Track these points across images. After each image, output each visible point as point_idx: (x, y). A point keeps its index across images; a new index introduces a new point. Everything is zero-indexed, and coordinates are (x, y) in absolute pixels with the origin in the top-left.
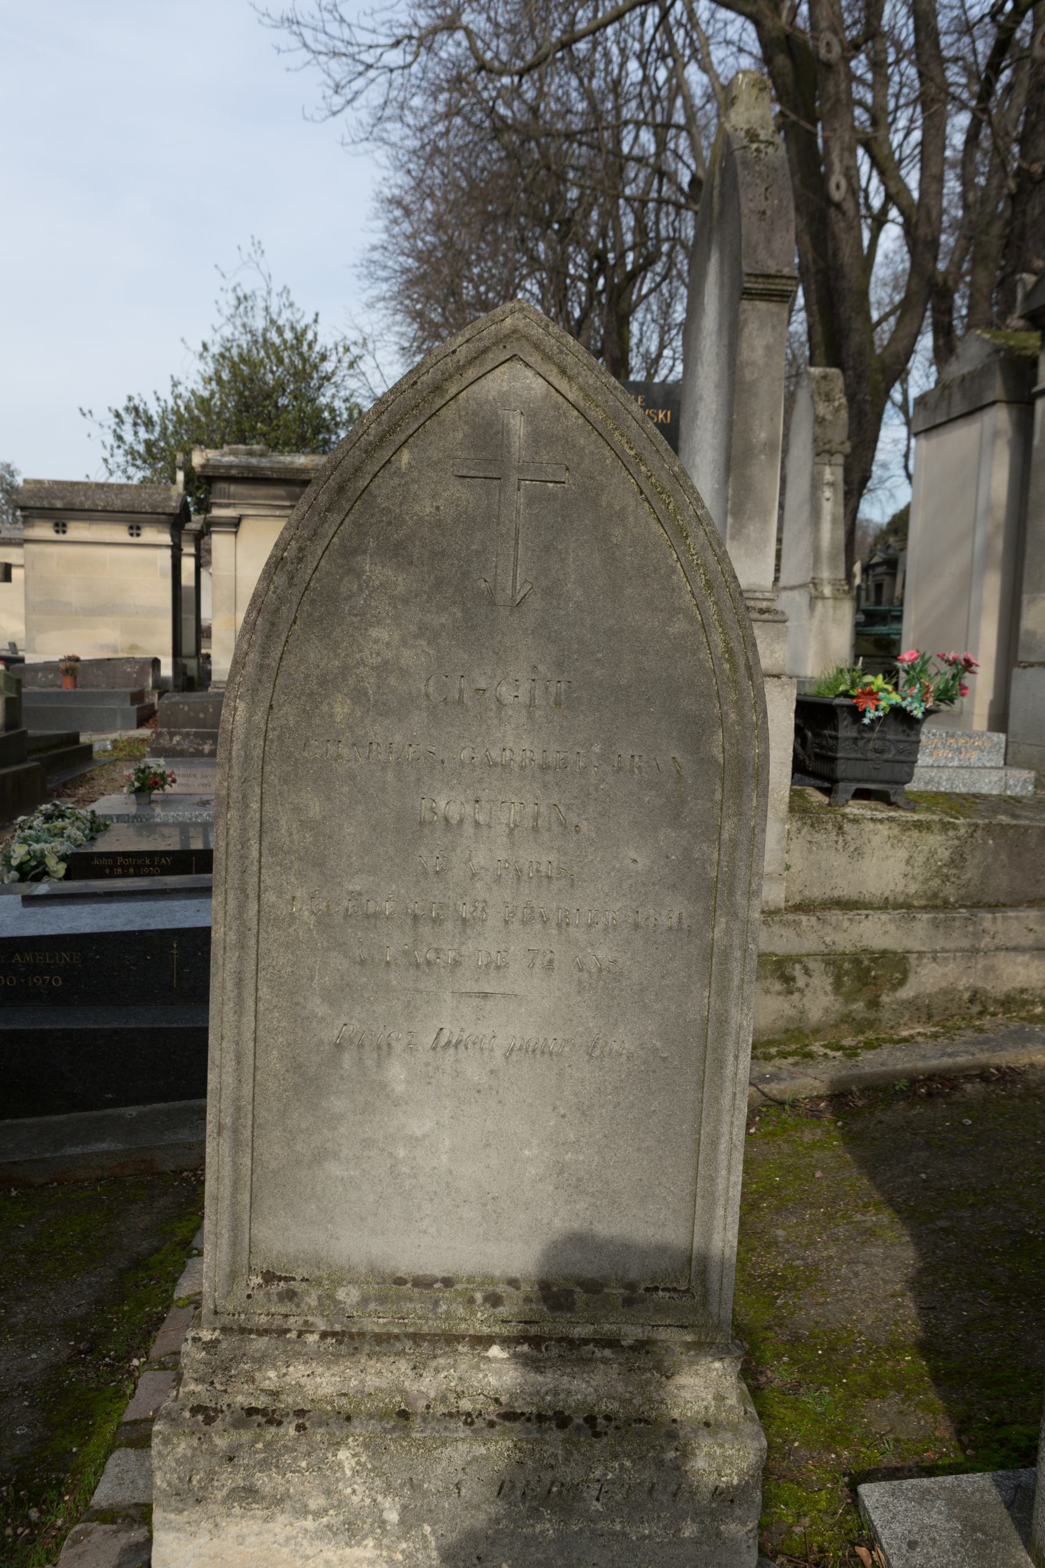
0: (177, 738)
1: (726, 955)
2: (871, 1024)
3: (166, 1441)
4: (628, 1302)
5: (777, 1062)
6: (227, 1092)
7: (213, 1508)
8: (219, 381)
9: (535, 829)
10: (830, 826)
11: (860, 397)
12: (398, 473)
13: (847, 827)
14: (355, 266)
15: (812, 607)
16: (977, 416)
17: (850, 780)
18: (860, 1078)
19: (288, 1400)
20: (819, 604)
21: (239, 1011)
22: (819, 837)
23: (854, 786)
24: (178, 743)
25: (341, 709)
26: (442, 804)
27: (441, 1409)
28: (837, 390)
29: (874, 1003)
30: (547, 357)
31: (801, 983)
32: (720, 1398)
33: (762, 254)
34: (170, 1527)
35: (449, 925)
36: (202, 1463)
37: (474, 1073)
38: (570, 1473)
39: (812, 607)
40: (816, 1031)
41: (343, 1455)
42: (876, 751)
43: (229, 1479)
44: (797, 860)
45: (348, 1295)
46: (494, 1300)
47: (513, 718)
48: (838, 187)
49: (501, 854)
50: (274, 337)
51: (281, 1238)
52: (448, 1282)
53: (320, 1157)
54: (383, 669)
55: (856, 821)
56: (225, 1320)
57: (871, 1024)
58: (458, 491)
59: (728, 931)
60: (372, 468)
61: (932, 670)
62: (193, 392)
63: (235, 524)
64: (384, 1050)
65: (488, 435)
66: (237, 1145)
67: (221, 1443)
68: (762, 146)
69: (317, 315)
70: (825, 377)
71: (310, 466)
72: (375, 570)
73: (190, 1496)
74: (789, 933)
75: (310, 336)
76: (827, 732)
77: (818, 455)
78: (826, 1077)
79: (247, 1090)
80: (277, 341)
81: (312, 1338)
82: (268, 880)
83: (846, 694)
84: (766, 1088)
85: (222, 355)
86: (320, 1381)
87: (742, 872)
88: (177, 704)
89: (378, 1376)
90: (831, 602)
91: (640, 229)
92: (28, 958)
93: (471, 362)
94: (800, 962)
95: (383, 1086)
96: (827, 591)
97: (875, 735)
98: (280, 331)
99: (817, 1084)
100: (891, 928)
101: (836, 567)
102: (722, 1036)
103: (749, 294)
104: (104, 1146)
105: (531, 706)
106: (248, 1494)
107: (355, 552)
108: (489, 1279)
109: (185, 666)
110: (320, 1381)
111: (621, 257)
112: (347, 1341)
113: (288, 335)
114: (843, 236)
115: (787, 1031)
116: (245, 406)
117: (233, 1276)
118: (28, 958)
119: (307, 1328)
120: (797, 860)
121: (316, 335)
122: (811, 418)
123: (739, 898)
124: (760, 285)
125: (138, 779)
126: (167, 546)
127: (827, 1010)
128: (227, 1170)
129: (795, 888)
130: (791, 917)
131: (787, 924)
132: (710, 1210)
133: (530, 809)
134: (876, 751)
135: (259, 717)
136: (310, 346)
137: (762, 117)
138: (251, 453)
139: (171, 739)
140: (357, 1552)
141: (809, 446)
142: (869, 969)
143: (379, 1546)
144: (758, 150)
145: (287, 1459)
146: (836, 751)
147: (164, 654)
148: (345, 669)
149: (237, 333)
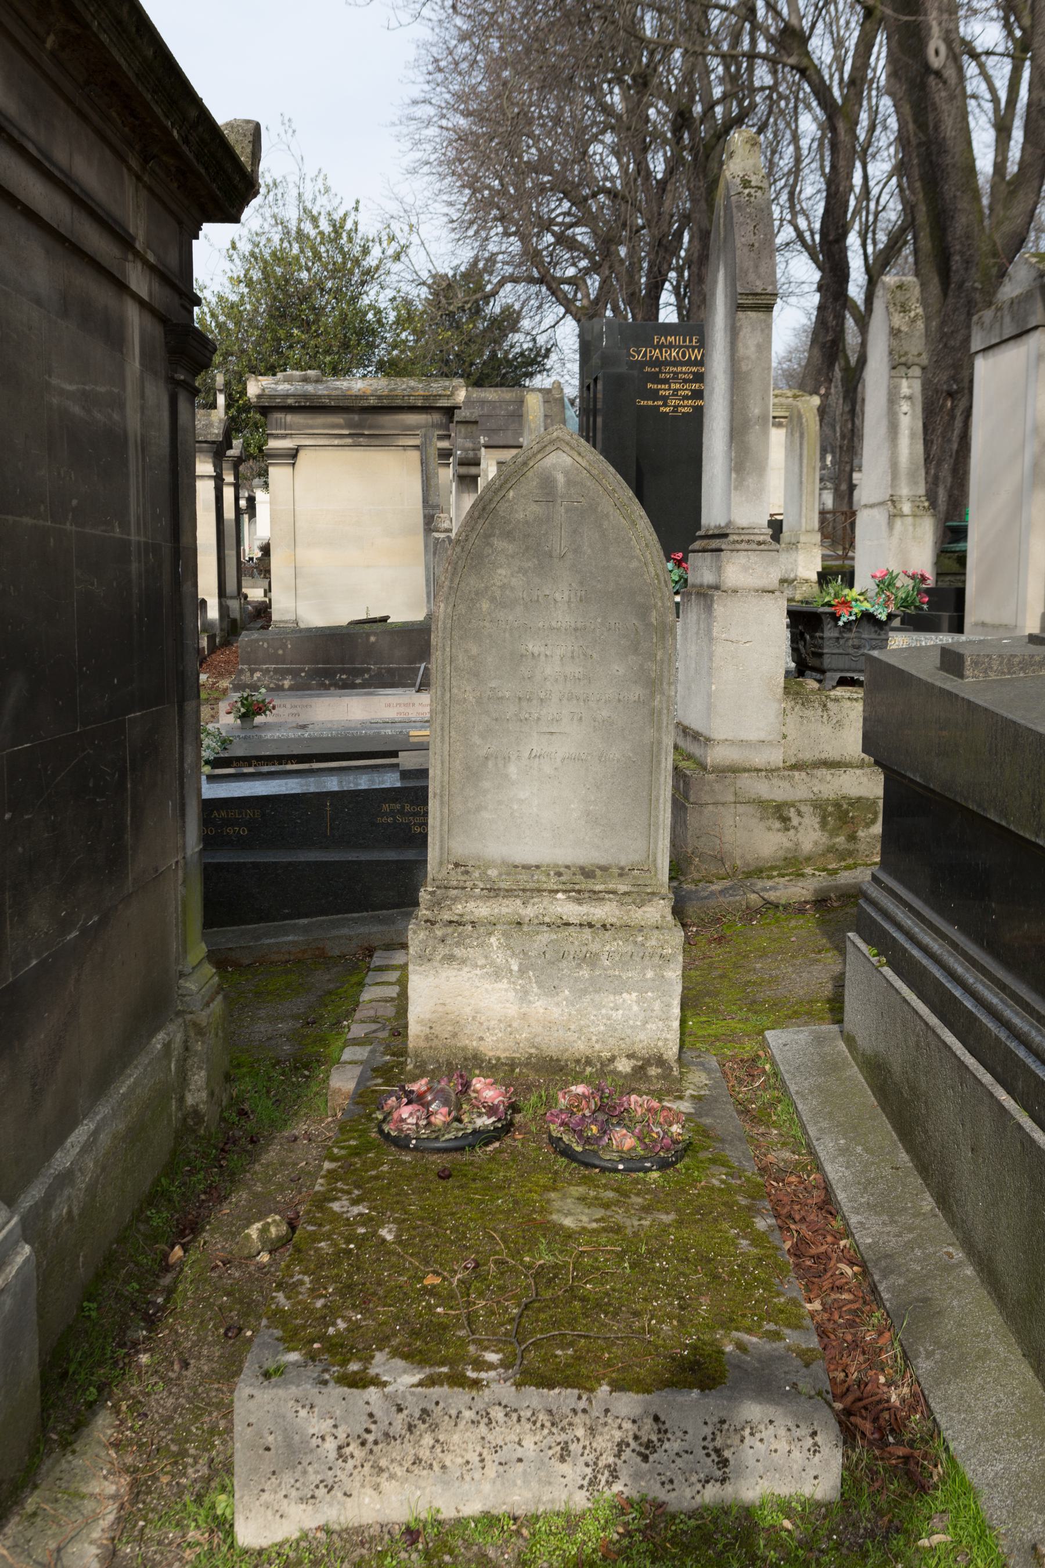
0: (257, 675)
1: (660, 712)
2: (850, 853)
3: (415, 932)
4: (621, 875)
5: (777, 880)
6: (438, 778)
7: (436, 964)
8: (250, 283)
9: (573, 657)
10: (816, 705)
11: (968, 284)
12: (508, 501)
13: (830, 705)
14: (393, 124)
15: (891, 525)
16: (1024, 338)
17: (835, 671)
18: (837, 888)
19: (467, 918)
20: (898, 522)
21: (443, 741)
22: (809, 713)
23: (838, 675)
24: (259, 679)
25: (485, 605)
26: (530, 647)
27: (536, 921)
28: (914, 299)
29: (852, 838)
30: (573, 448)
31: (795, 821)
32: (663, 917)
33: (752, 276)
34: (415, 972)
35: (535, 702)
36: (430, 942)
37: (548, 769)
38: (595, 947)
39: (891, 525)
40: (808, 859)
41: (493, 939)
42: (854, 647)
43: (442, 951)
44: (791, 730)
45: (493, 873)
46: (559, 874)
47: (560, 603)
48: (937, 53)
49: (558, 669)
50: (308, 228)
51: (462, 847)
52: (537, 867)
53: (479, 809)
54: (503, 587)
55: (836, 700)
56: (438, 883)
57: (850, 853)
58: (535, 508)
59: (661, 702)
60: (497, 499)
61: (899, 584)
62: (220, 298)
63: (293, 455)
64: (507, 759)
65: (547, 483)
66: (442, 803)
67: (439, 933)
68: (753, 191)
69: (357, 202)
70: (900, 287)
71: (369, 392)
72: (499, 543)
73: (425, 958)
74: (785, 784)
75: (349, 225)
76: (818, 634)
77: (894, 368)
78: (811, 888)
79: (446, 778)
80: (313, 233)
81: (477, 891)
82: (454, 683)
83: (828, 604)
84: (766, 895)
85: (252, 254)
86: (481, 910)
87: (666, 674)
88: (257, 641)
89: (509, 908)
90: (910, 520)
91: (731, 79)
92: (223, 814)
93: (539, 452)
94: (794, 806)
95: (507, 776)
96: (906, 508)
97: (852, 635)
98: (315, 220)
99: (804, 892)
100: (864, 780)
101: (916, 483)
102: (659, 749)
103: (741, 307)
104: (290, 938)
105: (569, 602)
106: (450, 958)
107: (490, 536)
108: (557, 866)
109: (228, 607)
110: (481, 910)
111: (709, 108)
112: (493, 892)
113: (325, 226)
114: (945, 107)
115: (786, 859)
116: (280, 314)
117: (441, 863)
118: (223, 814)
119: (475, 886)
120: (791, 730)
121: (356, 223)
122: (887, 330)
123: (665, 686)
124: (750, 301)
125: (243, 705)
126: (210, 477)
127: (816, 843)
128: (438, 814)
129: (791, 752)
130: (786, 773)
131: (783, 778)
132: (657, 831)
133: (570, 648)
134: (854, 647)
135: (449, 610)
136: (350, 240)
137: (754, 165)
138: (305, 380)
139: (252, 675)
140: (499, 985)
141: (886, 359)
142: (847, 812)
143: (509, 982)
144: (749, 195)
145: (468, 941)
146: (821, 648)
147: (209, 595)
148: (487, 588)
149: (266, 226)
